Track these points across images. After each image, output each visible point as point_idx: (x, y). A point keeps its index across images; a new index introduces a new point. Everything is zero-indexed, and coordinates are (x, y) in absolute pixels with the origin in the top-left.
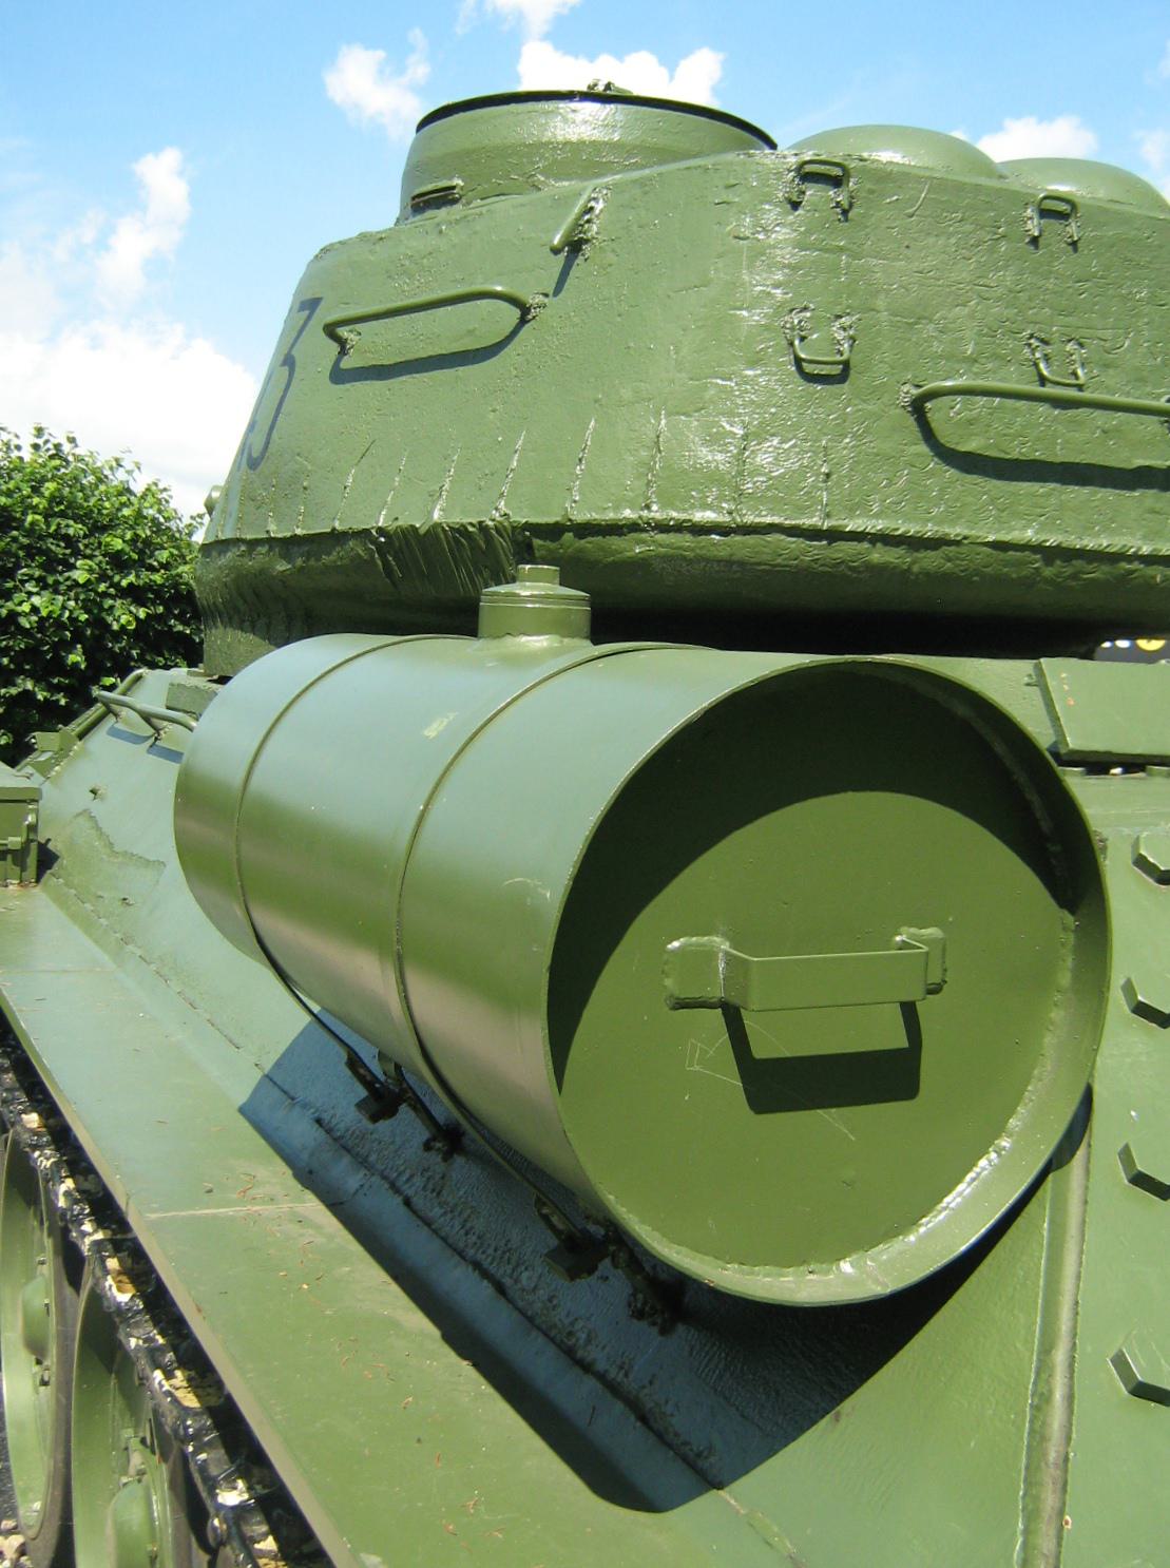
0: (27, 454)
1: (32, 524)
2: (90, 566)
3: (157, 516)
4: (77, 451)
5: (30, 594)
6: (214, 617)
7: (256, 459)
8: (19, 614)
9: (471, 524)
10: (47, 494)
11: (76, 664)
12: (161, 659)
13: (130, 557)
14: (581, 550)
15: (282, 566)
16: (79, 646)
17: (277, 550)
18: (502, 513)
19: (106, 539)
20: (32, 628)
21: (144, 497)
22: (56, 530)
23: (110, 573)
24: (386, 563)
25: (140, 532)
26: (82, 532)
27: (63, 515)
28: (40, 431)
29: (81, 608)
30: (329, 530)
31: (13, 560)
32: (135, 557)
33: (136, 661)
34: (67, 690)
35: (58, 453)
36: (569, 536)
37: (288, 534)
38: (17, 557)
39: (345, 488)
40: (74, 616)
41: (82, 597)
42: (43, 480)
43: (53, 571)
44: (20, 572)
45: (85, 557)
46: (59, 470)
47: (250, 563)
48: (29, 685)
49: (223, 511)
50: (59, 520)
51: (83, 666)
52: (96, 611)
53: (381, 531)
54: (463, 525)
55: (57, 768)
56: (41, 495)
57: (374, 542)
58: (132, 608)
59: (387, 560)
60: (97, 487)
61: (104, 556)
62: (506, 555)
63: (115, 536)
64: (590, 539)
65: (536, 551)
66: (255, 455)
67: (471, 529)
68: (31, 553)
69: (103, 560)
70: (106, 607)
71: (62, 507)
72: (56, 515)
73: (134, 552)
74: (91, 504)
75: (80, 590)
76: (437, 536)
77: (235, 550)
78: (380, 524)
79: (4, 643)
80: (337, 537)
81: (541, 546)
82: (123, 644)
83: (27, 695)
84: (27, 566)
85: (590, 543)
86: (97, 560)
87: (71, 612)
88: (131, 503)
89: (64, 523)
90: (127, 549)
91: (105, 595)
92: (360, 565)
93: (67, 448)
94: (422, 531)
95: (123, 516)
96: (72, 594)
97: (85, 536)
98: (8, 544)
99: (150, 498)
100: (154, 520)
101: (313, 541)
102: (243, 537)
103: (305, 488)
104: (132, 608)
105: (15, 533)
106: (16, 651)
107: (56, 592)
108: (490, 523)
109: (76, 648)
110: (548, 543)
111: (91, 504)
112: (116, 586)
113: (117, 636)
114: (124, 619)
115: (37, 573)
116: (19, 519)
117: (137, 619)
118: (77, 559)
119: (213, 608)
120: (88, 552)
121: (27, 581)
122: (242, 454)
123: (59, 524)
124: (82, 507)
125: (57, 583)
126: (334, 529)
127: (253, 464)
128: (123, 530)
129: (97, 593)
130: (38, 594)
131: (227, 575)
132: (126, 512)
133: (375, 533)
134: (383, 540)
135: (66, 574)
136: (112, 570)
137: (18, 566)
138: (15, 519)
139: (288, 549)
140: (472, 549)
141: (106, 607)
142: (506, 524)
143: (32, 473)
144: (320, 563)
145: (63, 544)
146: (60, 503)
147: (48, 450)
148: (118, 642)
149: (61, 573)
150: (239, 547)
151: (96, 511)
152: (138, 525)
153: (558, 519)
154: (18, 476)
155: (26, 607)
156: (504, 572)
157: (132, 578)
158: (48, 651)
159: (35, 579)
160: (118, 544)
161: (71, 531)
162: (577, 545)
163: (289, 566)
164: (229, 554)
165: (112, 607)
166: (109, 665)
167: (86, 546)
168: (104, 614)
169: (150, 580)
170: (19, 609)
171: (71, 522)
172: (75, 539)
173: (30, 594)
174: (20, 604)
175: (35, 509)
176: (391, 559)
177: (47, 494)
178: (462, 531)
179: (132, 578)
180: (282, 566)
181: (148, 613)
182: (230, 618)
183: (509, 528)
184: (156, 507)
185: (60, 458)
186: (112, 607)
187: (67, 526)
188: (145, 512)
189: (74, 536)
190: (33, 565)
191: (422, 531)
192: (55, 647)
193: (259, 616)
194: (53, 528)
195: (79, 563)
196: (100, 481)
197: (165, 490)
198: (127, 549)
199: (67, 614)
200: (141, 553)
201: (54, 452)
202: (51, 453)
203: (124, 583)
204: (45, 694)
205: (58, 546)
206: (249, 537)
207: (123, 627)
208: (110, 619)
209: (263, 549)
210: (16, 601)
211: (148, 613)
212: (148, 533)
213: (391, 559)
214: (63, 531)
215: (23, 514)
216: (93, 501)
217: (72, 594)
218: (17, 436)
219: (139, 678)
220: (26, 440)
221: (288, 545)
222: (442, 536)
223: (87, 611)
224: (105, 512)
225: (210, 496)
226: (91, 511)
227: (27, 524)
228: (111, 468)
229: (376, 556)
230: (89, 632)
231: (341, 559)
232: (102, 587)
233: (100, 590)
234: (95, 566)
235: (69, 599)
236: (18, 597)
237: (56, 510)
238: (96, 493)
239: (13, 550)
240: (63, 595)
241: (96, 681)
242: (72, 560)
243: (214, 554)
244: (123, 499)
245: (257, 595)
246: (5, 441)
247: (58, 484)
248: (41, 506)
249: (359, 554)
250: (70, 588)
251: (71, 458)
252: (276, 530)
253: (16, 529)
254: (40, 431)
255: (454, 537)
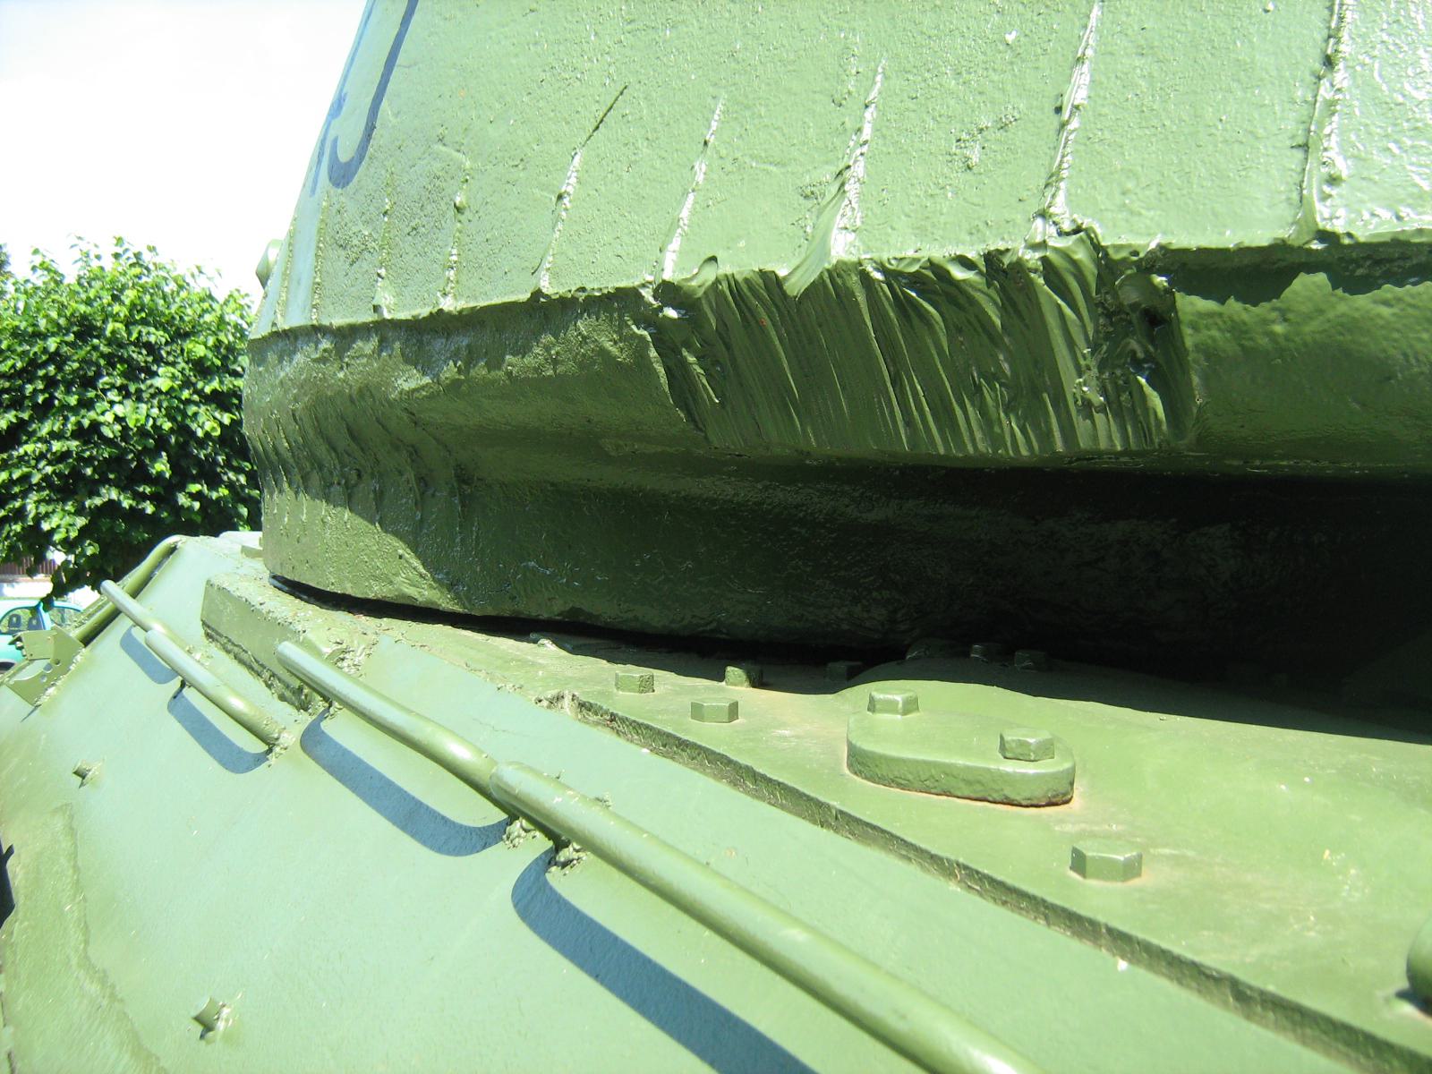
0: (108, 264)
1: (113, 332)
2: (173, 374)
3: (240, 321)
4: (157, 260)
5: (112, 403)
6: (275, 472)
7: (348, 164)
8: (102, 424)
9: (965, 262)
10: (127, 302)
11: (160, 474)
12: (248, 464)
13: (213, 363)
14: (1351, 325)
15: (410, 381)
16: (164, 454)
17: (397, 345)
18: (1067, 227)
19: (188, 345)
20: (115, 437)
21: (226, 303)
22: (137, 339)
23: (193, 379)
24: (678, 372)
25: (222, 337)
26: (163, 340)
27: (144, 322)
28: (119, 241)
29: (165, 416)
30: (524, 297)
31: (93, 369)
32: (218, 363)
33: (222, 467)
34: (152, 498)
35: (138, 261)
36: (1309, 286)
37: (424, 312)
38: (98, 365)
39: (560, 197)
40: (158, 424)
41: (165, 404)
42: (122, 291)
43: (136, 379)
44: (101, 381)
45: (167, 364)
46: (140, 278)
47: (341, 375)
48: (114, 494)
49: (285, 276)
50: (140, 327)
51: (167, 475)
52: (179, 419)
53: (668, 292)
54: (932, 265)
55: (51, 691)
56: (122, 303)
57: (650, 319)
58: (217, 415)
59: (684, 364)
60: (178, 293)
61: (187, 363)
62: (1071, 344)
63: (197, 342)
64: (1388, 290)
65: (1187, 331)
66: (344, 156)
67: (958, 273)
68: (111, 360)
69: (186, 367)
70: (190, 413)
71: (143, 315)
72: (135, 323)
73: (217, 358)
74: (173, 311)
75: (163, 397)
76: (844, 296)
77: (309, 348)
78: (668, 276)
79: (88, 453)
80: (543, 313)
81: (1211, 315)
82: (209, 450)
83: (112, 505)
84: (108, 374)
85: (1386, 303)
86: (179, 367)
87: (154, 419)
88: (213, 310)
89: (144, 331)
90: (210, 355)
91: (188, 402)
92: (602, 374)
93: (147, 258)
94: (795, 287)
95: (205, 322)
96: (155, 402)
97: (167, 343)
98: (89, 352)
99: (232, 305)
100: (236, 326)
101: (482, 324)
102: (326, 322)
103: (459, 209)
104: (217, 415)
105: (96, 341)
106: (99, 461)
107: (139, 400)
108: (1032, 258)
109: (161, 457)
110: (1234, 306)
111: (173, 311)
112: (200, 392)
113: (202, 443)
114: (208, 426)
115: (119, 382)
116: (100, 328)
117: (221, 424)
118: (159, 366)
119: (274, 457)
120: (171, 359)
121: (109, 390)
122: (319, 162)
123: (140, 332)
124: (163, 314)
125: (139, 391)
126: (537, 294)
127: (342, 174)
128: (206, 337)
129: (180, 400)
130: (120, 403)
131: (296, 400)
132: (208, 318)
133: (651, 300)
134: (671, 313)
135: (149, 382)
136: (195, 376)
137: (98, 375)
138: (95, 328)
139: (420, 342)
140: (954, 330)
141: (190, 413)
142: (1081, 255)
143: (112, 282)
144: (500, 374)
145: (144, 352)
146: (143, 310)
147: (128, 258)
148: (203, 448)
149: (143, 381)
150: (317, 343)
151: (178, 318)
152: (221, 331)
153: (1285, 233)
154: (97, 284)
155: (109, 417)
156: (1059, 399)
157: (215, 384)
158: (133, 459)
159: (117, 388)
160: (200, 351)
161: (152, 339)
162: (1342, 308)
163: (427, 380)
164: (299, 358)
165: (196, 414)
166: (194, 472)
167: (168, 353)
168: (188, 421)
169: (234, 386)
170: (101, 419)
171: (152, 330)
172: (157, 347)
173: (112, 403)
174: (103, 413)
175: (116, 317)
176: (692, 359)
177: (127, 302)
178: (933, 282)
179: (215, 384)
180: (410, 381)
181: (232, 419)
182: (305, 478)
183: (1090, 270)
184: (238, 313)
185: (141, 266)
186: (196, 414)
187: (148, 333)
188: (227, 319)
189: (156, 343)
190: (115, 373)
191: (795, 287)
192: (138, 455)
193: (359, 476)
194: (135, 335)
195: (161, 371)
196: (181, 287)
197: (247, 295)
198: (210, 355)
199: (151, 422)
200: (225, 359)
201: (135, 260)
202: (131, 261)
203: (208, 390)
204: (131, 502)
205: (140, 353)
206: (338, 321)
207: (207, 435)
208: (194, 426)
209: (368, 346)
210: (99, 411)
211: (232, 419)
212: (231, 338)
213: (692, 359)
214: (145, 339)
215: (103, 322)
216: (173, 309)
217: (155, 402)
218: (96, 246)
219: (172, 550)
220: (108, 249)
221: (421, 336)
222: (861, 297)
223: (171, 418)
224: (186, 319)
225: (265, 258)
226: (173, 318)
227: (108, 333)
228: (193, 276)
229: (653, 353)
230: (173, 440)
231: (555, 362)
232: (186, 394)
233: (183, 398)
234: (177, 373)
235: (152, 407)
236: (100, 406)
237: (137, 318)
238: (177, 300)
239: (94, 359)
240: (146, 403)
241: (182, 488)
242: (154, 368)
243: (271, 357)
244: (206, 305)
245: (353, 434)
246: (85, 251)
247: (138, 291)
248: (122, 315)
249: (603, 352)
250: (153, 396)
251: (152, 267)
252: (397, 305)
253: (98, 337)
254: (119, 241)
255: (903, 305)
